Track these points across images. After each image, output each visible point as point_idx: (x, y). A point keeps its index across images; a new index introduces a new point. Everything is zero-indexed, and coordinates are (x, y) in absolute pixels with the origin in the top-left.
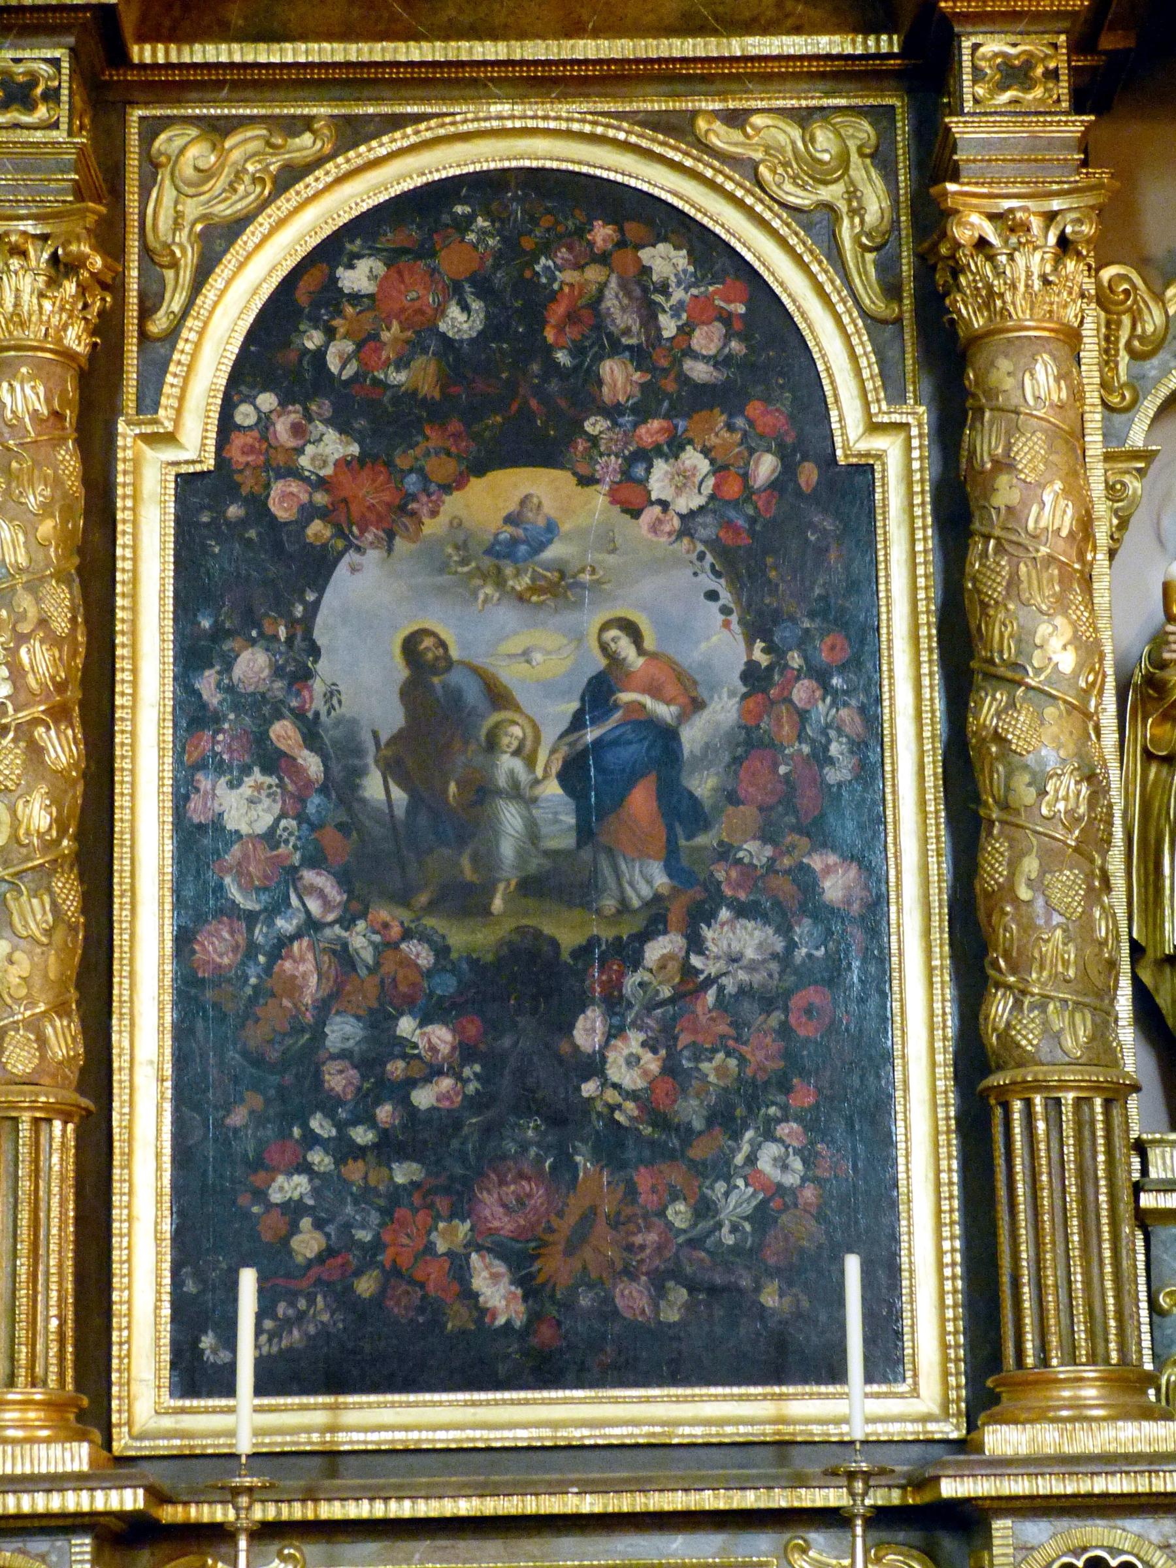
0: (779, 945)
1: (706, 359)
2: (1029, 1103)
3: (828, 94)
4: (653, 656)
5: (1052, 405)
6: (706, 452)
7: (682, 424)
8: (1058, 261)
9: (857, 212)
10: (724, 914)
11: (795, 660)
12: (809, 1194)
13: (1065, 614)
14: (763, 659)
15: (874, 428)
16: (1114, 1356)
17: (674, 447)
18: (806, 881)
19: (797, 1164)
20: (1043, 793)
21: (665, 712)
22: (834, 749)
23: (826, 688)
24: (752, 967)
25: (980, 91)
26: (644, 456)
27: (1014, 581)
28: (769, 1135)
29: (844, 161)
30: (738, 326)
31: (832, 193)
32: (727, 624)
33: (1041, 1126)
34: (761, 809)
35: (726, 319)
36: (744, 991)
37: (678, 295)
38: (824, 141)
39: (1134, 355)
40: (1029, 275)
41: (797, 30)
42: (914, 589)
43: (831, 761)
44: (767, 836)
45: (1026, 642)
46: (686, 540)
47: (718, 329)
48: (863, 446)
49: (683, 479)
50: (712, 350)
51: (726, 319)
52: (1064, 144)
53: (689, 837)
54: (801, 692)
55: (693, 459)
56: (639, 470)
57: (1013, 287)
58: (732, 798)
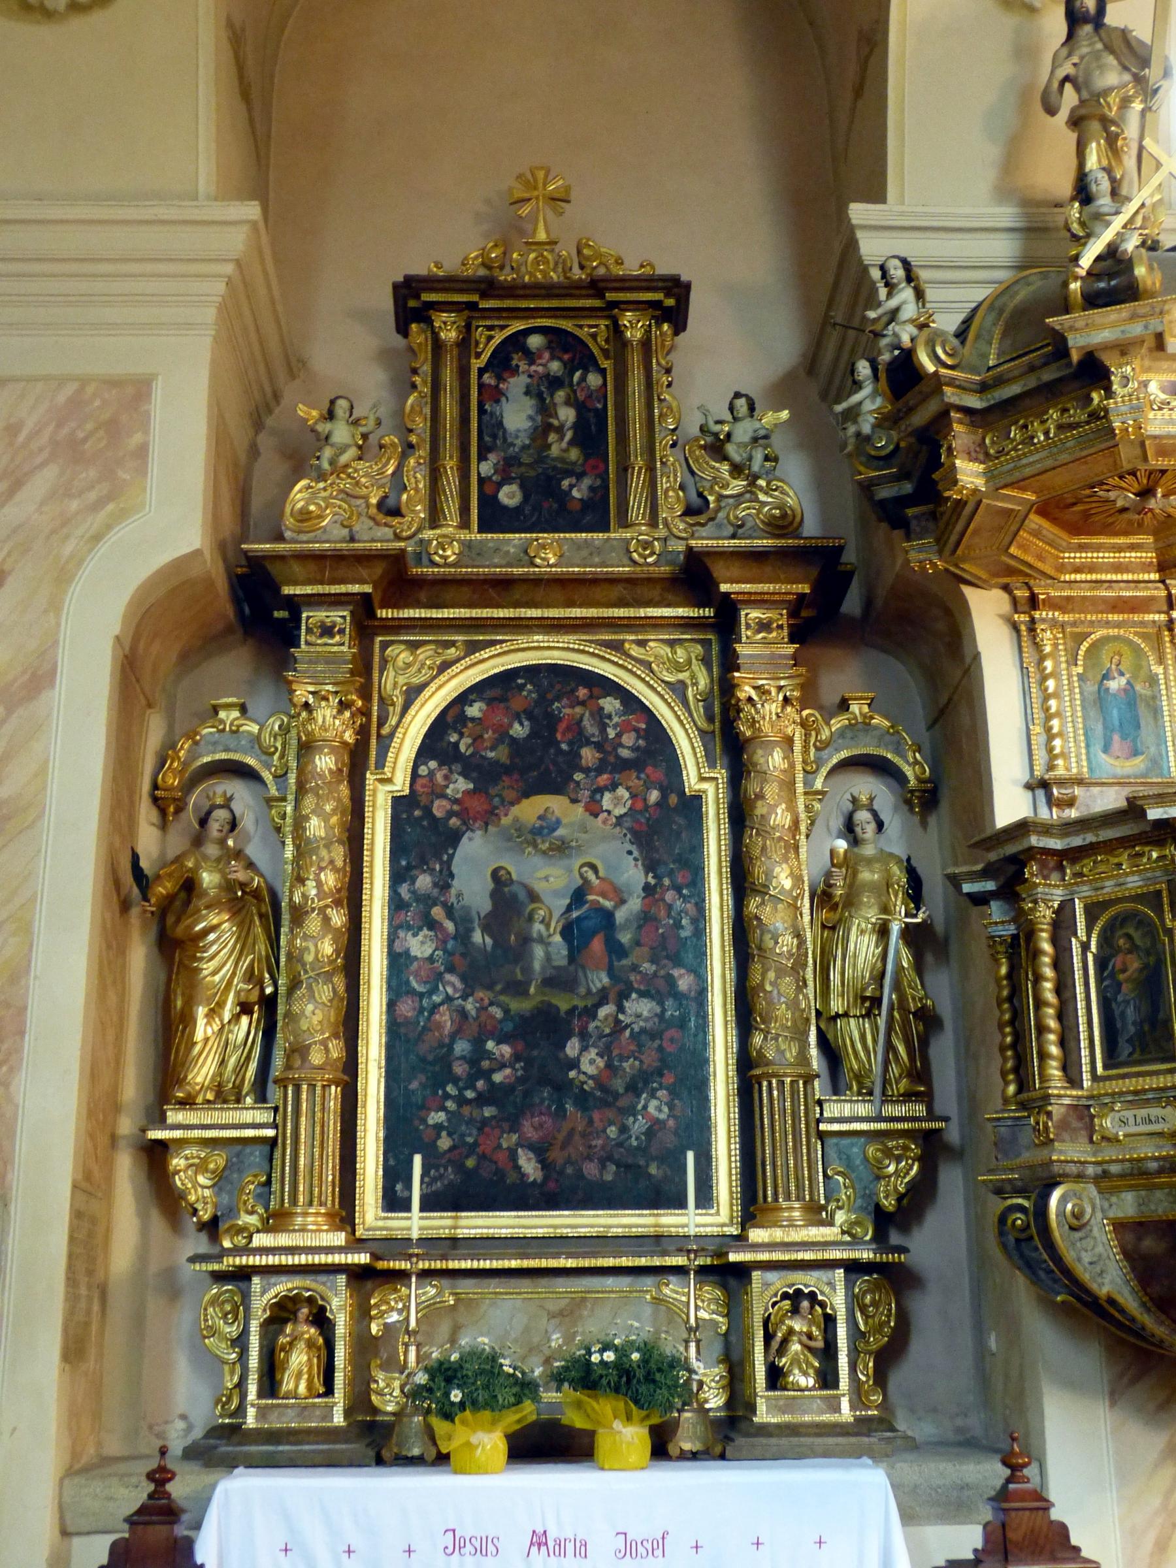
0: (658, 1010)
1: (628, 748)
2: (770, 1084)
3: (682, 633)
6: (628, 789)
7: (617, 776)
8: (783, 707)
9: (696, 684)
10: (634, 996)
11: (666, 882)
14: (652, 881)
16: (807, 1197)
17: (613, 787)
18: (671, 981)
19: (666, 1109)
21: (608, 904)
22: (684, 922)
23: (681, 895)
24: (646, 1020)
25: (749, 633)
26: (600, 790)
27: (764, 848)
29: (689, 662)
32: (636, 866)
33: (775, 1093)
37: (616, 719)
38: (681, 655)
39: (817, 749)
41: (668, 605)
43: (682, 927)
45: (769, 875)
47: (633, 735)
48: (697, 787)
49: (617, 801)
51: (637, 730)
54: (670, 896)
55: (622, 792)
56: (598, 797)
57: (764, 718)
58: (638, 943)
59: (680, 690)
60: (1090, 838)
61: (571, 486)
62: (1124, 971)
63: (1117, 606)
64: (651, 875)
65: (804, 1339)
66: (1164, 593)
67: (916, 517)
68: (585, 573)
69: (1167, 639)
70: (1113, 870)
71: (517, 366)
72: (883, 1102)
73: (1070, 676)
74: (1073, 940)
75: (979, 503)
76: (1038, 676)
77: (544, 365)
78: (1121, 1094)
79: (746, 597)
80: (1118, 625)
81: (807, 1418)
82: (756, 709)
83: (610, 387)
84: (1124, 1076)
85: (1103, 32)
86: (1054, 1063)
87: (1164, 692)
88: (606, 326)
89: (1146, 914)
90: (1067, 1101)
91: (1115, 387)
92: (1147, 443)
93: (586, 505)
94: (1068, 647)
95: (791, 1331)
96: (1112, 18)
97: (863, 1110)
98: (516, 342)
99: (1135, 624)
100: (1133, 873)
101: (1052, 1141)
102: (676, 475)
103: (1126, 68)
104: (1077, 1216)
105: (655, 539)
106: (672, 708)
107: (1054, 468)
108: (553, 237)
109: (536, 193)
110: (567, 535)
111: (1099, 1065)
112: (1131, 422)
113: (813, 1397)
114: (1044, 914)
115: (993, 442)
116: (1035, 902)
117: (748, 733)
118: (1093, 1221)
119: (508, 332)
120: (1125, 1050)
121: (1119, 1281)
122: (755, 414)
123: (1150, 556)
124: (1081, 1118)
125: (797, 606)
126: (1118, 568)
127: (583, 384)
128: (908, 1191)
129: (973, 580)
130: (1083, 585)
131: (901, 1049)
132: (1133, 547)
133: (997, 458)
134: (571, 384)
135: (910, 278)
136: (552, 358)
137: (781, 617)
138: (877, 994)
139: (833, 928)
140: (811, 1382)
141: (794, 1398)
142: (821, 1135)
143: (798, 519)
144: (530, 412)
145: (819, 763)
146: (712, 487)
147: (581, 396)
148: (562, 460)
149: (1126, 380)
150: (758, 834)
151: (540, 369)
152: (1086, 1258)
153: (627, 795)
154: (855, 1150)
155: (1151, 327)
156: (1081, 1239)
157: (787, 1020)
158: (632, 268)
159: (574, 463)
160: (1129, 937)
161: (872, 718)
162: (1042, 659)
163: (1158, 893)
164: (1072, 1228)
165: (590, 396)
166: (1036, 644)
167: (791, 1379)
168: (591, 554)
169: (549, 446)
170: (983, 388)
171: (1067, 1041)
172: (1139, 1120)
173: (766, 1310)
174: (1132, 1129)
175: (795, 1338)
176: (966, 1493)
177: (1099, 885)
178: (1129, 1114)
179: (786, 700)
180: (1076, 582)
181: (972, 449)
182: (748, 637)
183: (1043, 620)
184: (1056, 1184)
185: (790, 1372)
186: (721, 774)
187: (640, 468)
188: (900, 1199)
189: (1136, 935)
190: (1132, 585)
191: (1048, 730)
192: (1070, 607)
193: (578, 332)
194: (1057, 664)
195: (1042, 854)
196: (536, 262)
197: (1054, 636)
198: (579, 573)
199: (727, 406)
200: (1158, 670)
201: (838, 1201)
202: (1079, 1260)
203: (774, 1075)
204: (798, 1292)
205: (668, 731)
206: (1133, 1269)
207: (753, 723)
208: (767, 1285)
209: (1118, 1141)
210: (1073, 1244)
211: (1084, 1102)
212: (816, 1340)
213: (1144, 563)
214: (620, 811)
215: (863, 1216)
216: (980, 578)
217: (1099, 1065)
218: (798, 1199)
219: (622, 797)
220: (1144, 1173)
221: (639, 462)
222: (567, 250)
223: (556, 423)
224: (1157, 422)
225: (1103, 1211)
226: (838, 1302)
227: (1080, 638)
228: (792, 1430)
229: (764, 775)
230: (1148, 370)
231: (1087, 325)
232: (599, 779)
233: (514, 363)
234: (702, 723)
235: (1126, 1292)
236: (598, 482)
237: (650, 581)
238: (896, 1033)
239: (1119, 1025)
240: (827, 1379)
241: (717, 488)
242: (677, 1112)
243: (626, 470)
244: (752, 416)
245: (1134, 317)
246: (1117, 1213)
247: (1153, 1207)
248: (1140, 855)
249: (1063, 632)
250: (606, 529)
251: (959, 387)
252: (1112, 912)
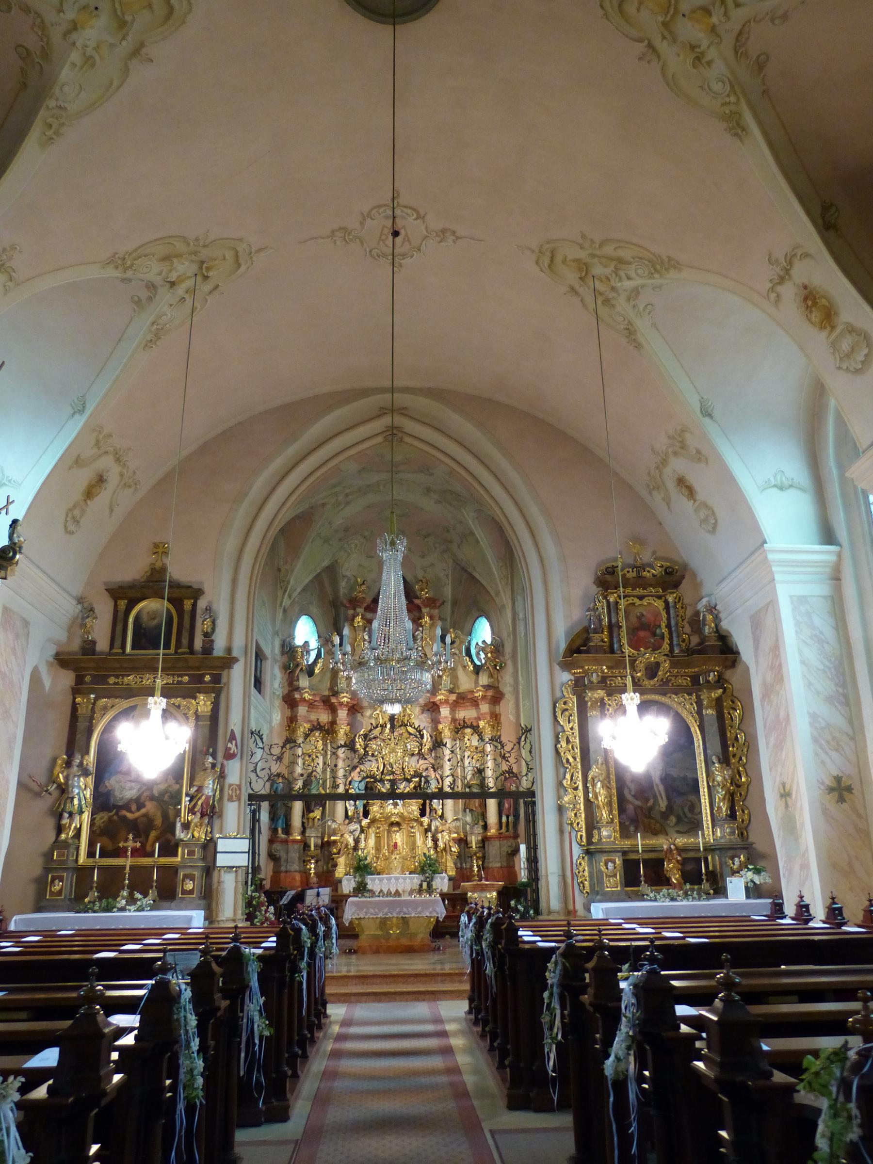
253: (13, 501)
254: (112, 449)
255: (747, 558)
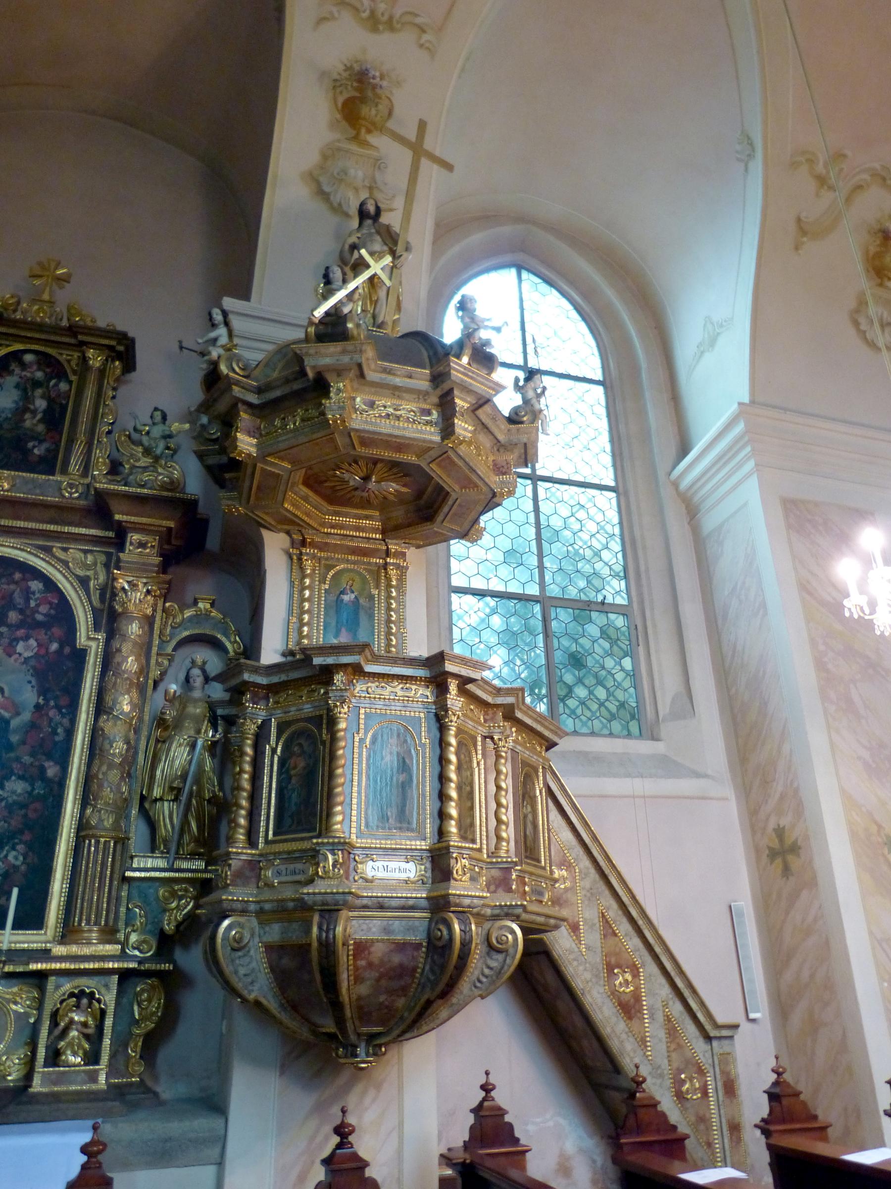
0: (29, 789)
1: (42, 614)
2: (90, 841)
3: (94, 546)
4: (7, 698)
5: (137, 635)
6: (36, 640)
7: (30, 631)
8: (146, 596)
9: (97, 579)
10: (13, 778)
11: (52, 703)
12: (23, 868)
13: (129, 694)
14: (41, 701)
15: (89, 638)
16: (103, 923)
17: (26, 638)
18: (42, 770)
19: (21, 858)
20: (112, 746)
21: (7, 715)
22: (59, 730)
23: (60, 712)
24: (20, 795)
25: (131, 548)
26: (17, 640)
27: (115, 683)
28: (14, 849)
29: (95, 564)
30: (54, 606)
31: (90, 573)
32: (33, 691)
33: (93, 849)
34: (32, 747)
35: (50, 603)
36: (15, 802)
37: (37, 595)
38: (90, 559)
39: (172, 627)
40: (136, 598)
41: (86, 527)
42: (92, 685)
43: (57, 734)
44: (32, 755)
45: (115, 702)
46: (25, 666)
47: (48, 606)
48: (85, 643)
49: (27, 648)
50: (45, 612)
51: (50, 603)
52: (153, 565)
53: (6, 754)
54: (52, 713)
55: (33, 642)
56: (15, 643)
57: (130, 601)
58: (24, 743)
59: (84, 582)
60: (283, 677)
61: (34, 447)
62: (295, 768)
63: (355, 551)
64: (41, 698)
65: (79, 1027)
66: (384, 548)
67: (230, 479)
68: (27, 498)
69: (383, 574)
70: (297, 700)
71: (13, 370)
72: (175, 859)
73: (320, 589)
74: (267, 746)
75: (255, 466)
76: (300, 588)
77: (32, 373)
78: (280, 853)
79: (132, 526)
80: (354, 563)
81: (73, 1088)
82: (126, 595)
83: (73, 392)
84: (285, 841)
85: (376, 224)
86: (241, 831)
87: (377, 605)
88: (79, 356)
89: (314, 732)
90: (244, 857)
91: (331, 394)
92: (352, 434)
93: (42, 459)
94: (322, 572)
95: (72, 1021)
96: (384, 219)
97: (161, 863)
98: (16, 356)
99: (364, 563)
100: (307, 702)
101: (229, 885)
102: (106, 450)
103: (386, 244)
104: (238, 941)
105: (80, 483)
106: (77, 592)
107: (297, 446)
108: (53, 300)
109: (48, 273)
110: (20, 474)
111: (271, 833)
112: (338, 416)
113: (79, 1071)
114: (251, 728)
115: (265, 427)
116: (245, 719)
117: (120, 610)
118: (251, 944)
119: (10, 349)
120: (288, 821)
121: (265, 988)
122: (167, 422)
123: (377, 524)
124: (252, 870)
125: (167, 536)
126: (358, 528)
127: (56, 388)
128: (184, 920)
129: (268, 525)
130: (336, 537)
131: (194, 825)
132: (367, 517)
133: (265, 436)
134: (48, 387)
135: (227, 324)
136: (39, 369)
137: (153, 541)
138: (181, 785)
139: (164, 742)
140: (79, 1060)
141: (64, 1073)
142: (125, 879)
143: (182, 486)
144: (16, 398)
145: (172, 636)
146: (128, 461)
147: (53, 394)
148: (32, 430)
149: (339, 390)
150: (113, 675)
151: (28, 375)
152: (242, 971)
153: (35, 644)
154: (152, 891)
155: (354, 359)
156: (240, 957)
157: (110, 799)
158: (101, 323)
159: (40, 434)
160: (300, 745)
161: (211, 612)
162: (304, 577)
163: (321, 716)
164: (233, 949)
165: (59, 395)
166: (301, 568)
167: (64, 1057)
168: (35, 488)
169: (24, 421)
170: (259, 391)
171: (253, 816)
172: (288, 872)
173: (55, 1005)
174: (284, 879)
175: (74, 1027)
176: (168, 1144)
177: (287, 710)
178: (283, 867)
179: (148, 592)
180: (331, 534)
181: (252, 430)
182: (129, 550)
183: (307, 554)
184: (226, 917)
185: (64, 1053)
186: (101, 636)
187: (82, 442)
188: (178, 927)
189: (305, 745)
190: (366, 540)
191: (301, 620)
192: (326, 549)
193: (59, 357)
194: (312, 581)
195: (255, 687)
196: (38, 311)
197: (314, 564)
198: (23, 498)
199: (150, 414)
200: (375, 592)
201: (133, 926)
202: (236, 972)
203: (94, 836)
204: (82, 992)
205: (73, 606)
206: (276, 979)
207: (123, 604)
208: (58, 987)
209: (274, 886)
210: (233, 961)
211: (256, 858)
212: (90, 1027)
213: (373, 528)
214: (28, 654)
215: (148, 937)
216: (270, 524)
217: (271, 833)
218: (95, 924)
219: (32, 645)
220: (285, 910)
221: (82, 438)
222: (61, 308)
223: (32, 407)
224: (357, 421)
225: (260, 936)
226: (109, 998)
227: (329, 568)
228: (54, 1098)
229: (124, 637)
230: (355, 390)
231: (316, 353)
232: (18, 632)
233: (11, 368)
234: (96, 602)
235: (270, 996)
236: (53, 447)
237: (72, 509)
238: (192, 812)
239: (287, 805)
240: (92, 1058)
241: (132, 461)
242: (29, 860)
243: (73, 441)
244: (164, 423)
245: (344, 352)
246: (268, 939)
247: (290, 935)
248: (313, 691)
249: (320, 563)
250: (53, 474)
251: (243, 388)
252: (293, 728)
253: (422, 126)
254: (866, 176)
255: (817, 416)
